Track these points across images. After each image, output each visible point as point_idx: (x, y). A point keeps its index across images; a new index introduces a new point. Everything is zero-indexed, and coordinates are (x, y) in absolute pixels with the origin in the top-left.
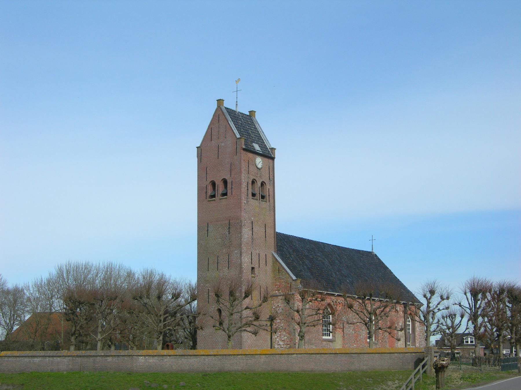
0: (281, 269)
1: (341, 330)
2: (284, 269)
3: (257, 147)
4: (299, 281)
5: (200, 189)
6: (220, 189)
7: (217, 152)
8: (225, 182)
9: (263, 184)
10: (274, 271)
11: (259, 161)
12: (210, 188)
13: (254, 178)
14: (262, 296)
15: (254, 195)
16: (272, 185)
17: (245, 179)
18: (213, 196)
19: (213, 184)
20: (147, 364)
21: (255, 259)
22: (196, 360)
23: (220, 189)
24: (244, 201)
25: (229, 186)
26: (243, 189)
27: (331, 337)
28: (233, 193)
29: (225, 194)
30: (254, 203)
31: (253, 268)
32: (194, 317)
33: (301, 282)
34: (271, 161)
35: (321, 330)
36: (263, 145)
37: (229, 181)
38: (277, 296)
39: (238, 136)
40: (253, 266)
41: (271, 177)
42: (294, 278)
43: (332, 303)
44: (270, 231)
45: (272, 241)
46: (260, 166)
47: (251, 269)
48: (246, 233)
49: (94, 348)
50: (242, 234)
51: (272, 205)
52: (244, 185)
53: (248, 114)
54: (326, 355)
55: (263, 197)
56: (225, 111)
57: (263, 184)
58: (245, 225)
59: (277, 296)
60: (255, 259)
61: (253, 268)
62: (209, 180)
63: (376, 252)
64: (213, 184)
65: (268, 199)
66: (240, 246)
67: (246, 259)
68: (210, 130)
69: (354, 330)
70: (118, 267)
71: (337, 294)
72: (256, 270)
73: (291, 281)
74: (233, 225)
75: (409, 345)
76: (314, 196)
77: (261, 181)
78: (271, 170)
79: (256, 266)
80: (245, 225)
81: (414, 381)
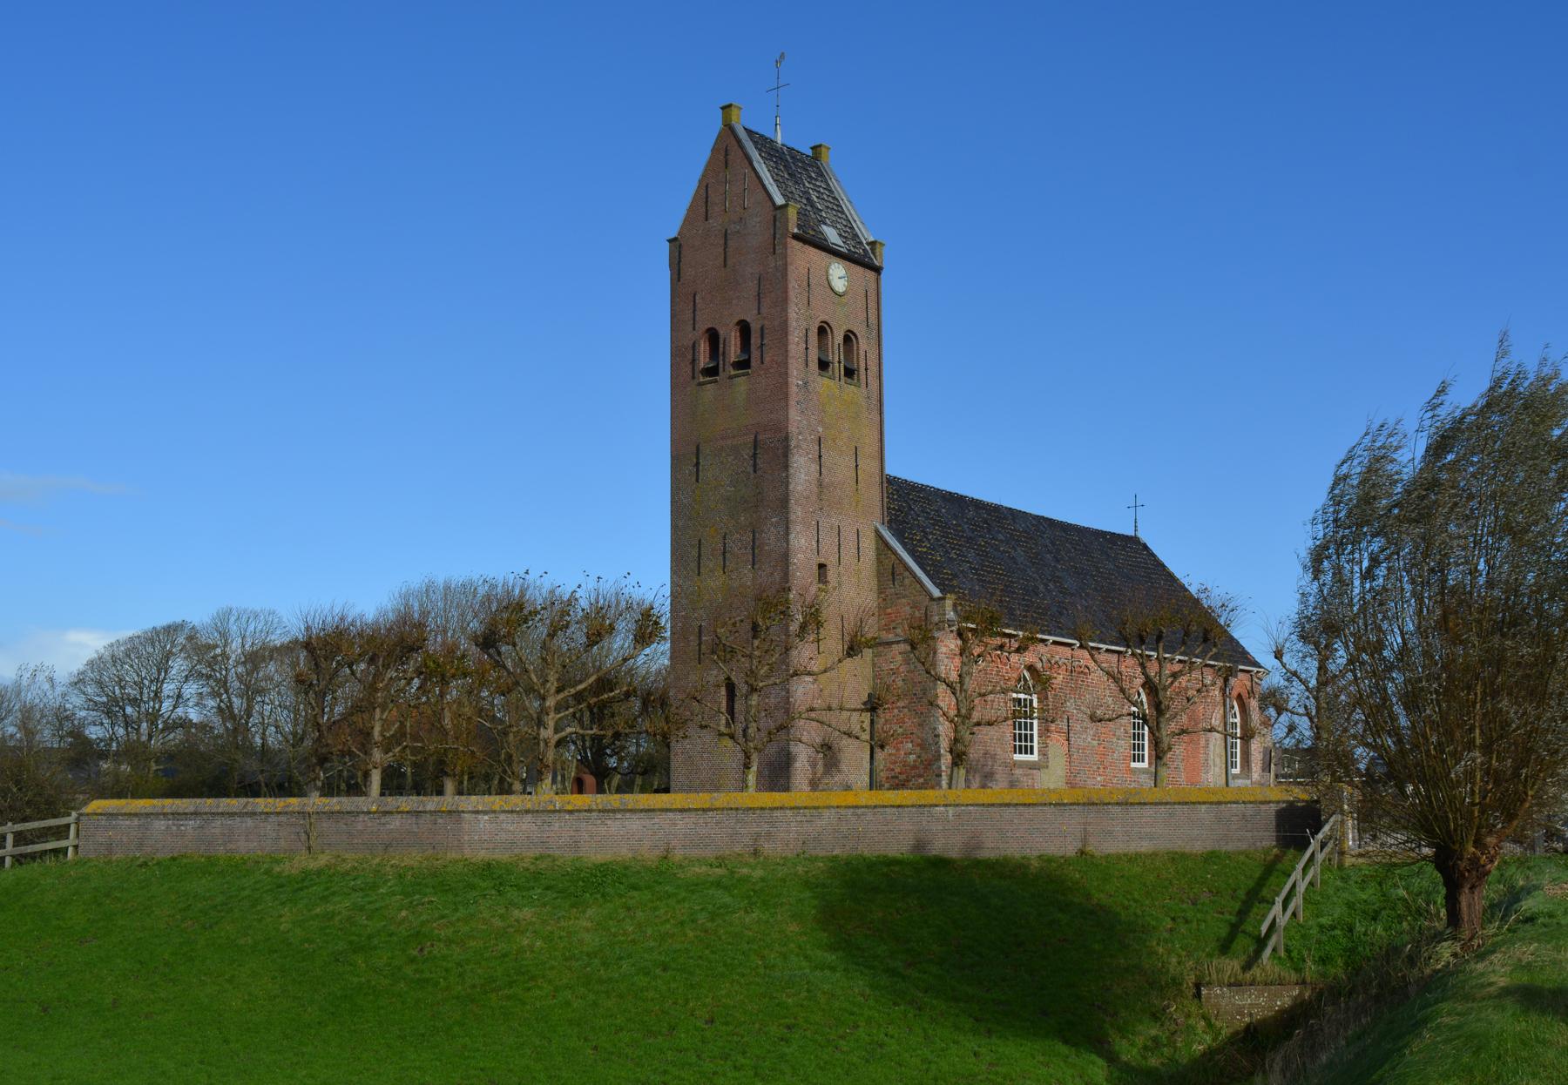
0: (900, 569)
1: (1062, 739)
2: (907, 568)
3: (832, 235)
4: (949, 603)
5: (680, 354)
6: (733, 351)
7: (721, 250)
8: (744, 329)
9: (849, 338)
10: (879, 575)
11: (838, 274)
12: (703, 347)
13: (826, 318)
14: (847, 638)
15: (823, 365)
16: (874, 342)
17: (799, 321)
18: (712, 372)
19: (713, 337)
20: (504, 836)
21: (828, 542)
22: (648, 823)
23: (733, 351)
24: (795, 380)
25: (755, 340)
26: (792, 347)
27: (1035, 757)
28: (767, 359)
29: (743, 365)
30: (827, 386)
31: (822, 566)
32: (654, 700)
33: (955, 605)
34: (871, 275)
35: (1009, 737)
36: (850, 234)
37: (755, 327)
38: (889, 644)
39: (779, 200)
40: (823, 561)
41: (873, 320)
42: (936, 593)
43: (1039, 665)
44: (868, 466)
45: (873, 496)
46: (840, 286)
47: (815, 567)
48: (802, 471)
49: (356, 788)
50: (792, 471)
51: (875, 395)
52: (795, 338)
53: (810, 153)
54: (1031, 809)
55: (849, 373)
56: (743, 135)
57: (849, 338)
58: (798, 446)
59: (889, 644)
60: (828, 542)
61: (822, 566)
62: (702, 326)
63: (1144, 537)
64: (713, 337)
65: (863, 377)
66: (784, 503)
67: (801, 544)
68: (703, 191)
69: (1096, 736)
70: (517, 592)
71: (1052, 638)
72: (831, 575)
73: (926, 601)
74: (768, 452)
75: (1235, 777)
76: (971, 413)
77: (845, 328)
78: (873, 301)
79: (831, 561)
80: (798, 446)
81: (1302, 887)
